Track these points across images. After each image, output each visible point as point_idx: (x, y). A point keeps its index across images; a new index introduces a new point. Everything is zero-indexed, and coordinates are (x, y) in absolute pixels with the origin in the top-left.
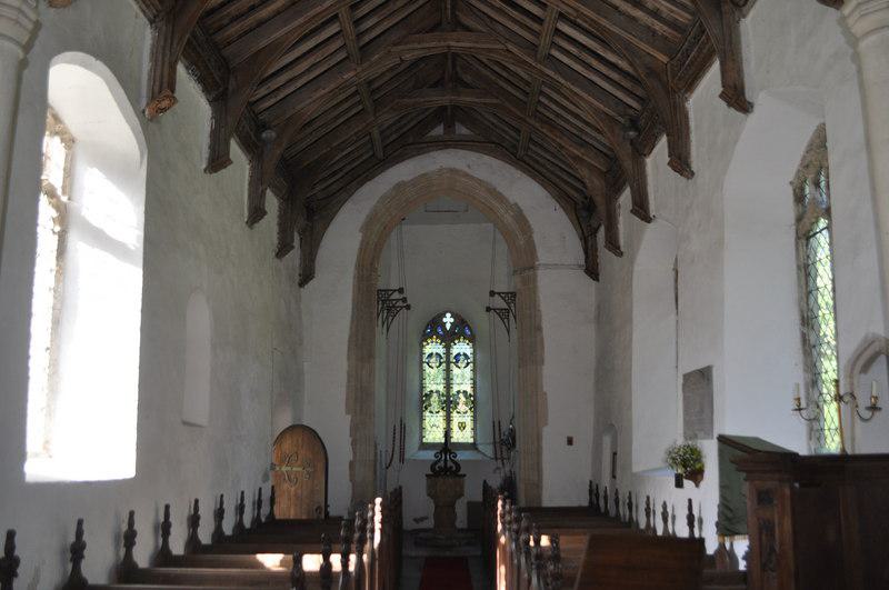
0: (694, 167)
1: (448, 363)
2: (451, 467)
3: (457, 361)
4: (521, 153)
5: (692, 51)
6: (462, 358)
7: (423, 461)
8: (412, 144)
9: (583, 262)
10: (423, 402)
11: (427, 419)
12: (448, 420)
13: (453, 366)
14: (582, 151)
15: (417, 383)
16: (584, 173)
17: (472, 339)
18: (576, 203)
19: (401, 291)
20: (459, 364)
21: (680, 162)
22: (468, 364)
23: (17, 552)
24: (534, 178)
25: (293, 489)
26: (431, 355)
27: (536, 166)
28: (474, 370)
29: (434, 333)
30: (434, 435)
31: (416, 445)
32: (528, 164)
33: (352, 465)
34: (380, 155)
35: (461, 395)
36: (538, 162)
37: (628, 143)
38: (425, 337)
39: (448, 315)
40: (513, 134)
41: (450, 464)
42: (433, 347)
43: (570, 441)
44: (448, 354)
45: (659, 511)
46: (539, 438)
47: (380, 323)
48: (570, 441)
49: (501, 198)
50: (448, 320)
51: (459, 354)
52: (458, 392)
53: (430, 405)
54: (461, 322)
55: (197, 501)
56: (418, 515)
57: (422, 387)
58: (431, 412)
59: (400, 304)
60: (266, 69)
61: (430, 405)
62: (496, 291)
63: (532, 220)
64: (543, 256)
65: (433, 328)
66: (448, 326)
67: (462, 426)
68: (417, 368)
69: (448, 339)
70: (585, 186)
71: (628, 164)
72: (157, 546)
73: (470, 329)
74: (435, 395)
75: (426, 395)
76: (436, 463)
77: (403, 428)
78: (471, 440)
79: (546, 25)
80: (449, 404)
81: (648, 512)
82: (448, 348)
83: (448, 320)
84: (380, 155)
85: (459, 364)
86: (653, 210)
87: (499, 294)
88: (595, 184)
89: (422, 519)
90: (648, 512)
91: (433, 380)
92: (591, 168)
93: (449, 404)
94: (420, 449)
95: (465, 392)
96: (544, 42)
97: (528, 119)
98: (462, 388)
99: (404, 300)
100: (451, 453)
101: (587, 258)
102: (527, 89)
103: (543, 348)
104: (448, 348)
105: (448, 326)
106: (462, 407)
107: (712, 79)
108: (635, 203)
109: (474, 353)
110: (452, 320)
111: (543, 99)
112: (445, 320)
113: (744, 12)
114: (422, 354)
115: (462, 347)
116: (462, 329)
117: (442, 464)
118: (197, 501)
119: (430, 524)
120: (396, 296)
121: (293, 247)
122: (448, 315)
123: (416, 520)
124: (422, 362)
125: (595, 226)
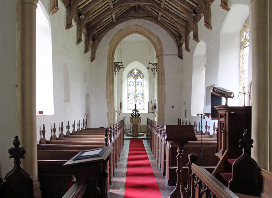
14: (178, 19)
19: (121, 63)
21: (208, 24)
22: (142, 85)
33: (108, 113)
34: (115, 21)
37: (193, 18)
39: (136, 70)
41: (137, 114)
43: (173, 107)
47: (115, 72)
48: (173, 107)
49: (152, 34)
50: (136, 72)
53: (130, 97)
64: (165, 52)
66: (135, 73)
71: (192, 24)
76: (133, 113)
83: (136, 72)
88: (182, 30)
92: (181, 25)
97: (161, 10)
99: (122, 65)
105: (135, 73)
110: (137, 71)
112: (134, 71)
117: (134, 114)
122: (136, 70)
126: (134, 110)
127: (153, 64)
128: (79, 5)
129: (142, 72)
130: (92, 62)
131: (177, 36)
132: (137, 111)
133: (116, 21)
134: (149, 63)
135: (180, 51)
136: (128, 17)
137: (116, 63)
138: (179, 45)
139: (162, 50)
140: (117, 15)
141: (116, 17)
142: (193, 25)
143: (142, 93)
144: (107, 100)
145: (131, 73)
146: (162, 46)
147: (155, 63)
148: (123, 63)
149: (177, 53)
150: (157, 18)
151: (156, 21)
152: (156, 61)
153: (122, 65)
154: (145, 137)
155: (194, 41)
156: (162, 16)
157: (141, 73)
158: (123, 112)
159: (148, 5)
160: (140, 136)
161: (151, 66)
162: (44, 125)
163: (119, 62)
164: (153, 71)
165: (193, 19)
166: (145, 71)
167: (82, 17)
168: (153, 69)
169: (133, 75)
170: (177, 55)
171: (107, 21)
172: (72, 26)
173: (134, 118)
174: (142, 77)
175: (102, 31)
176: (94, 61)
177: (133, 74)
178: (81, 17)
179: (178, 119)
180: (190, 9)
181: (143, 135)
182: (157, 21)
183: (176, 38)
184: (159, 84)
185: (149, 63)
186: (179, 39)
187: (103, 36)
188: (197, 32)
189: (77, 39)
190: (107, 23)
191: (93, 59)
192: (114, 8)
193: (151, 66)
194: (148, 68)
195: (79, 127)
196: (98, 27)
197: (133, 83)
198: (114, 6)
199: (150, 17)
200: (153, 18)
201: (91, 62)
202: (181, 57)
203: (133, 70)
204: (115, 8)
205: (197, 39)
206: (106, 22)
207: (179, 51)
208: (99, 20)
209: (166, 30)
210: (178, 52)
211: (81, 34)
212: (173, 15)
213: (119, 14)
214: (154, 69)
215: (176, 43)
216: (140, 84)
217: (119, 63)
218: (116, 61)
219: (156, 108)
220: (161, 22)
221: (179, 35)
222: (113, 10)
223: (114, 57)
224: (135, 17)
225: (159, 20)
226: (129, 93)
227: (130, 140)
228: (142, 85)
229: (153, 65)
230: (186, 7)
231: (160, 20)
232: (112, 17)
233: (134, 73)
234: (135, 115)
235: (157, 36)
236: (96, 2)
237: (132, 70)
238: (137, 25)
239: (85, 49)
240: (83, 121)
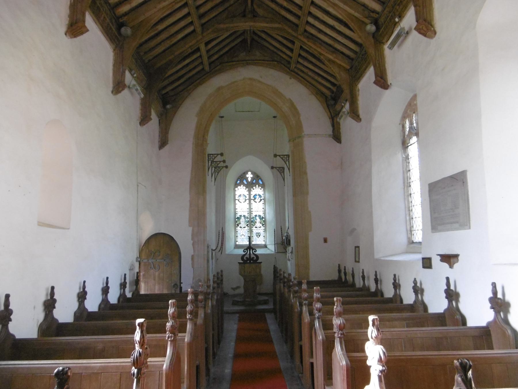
0: (361, 117)
1: (250, 199)
2: (254, 258)
3: (255, 199)
4: (293, 66)
5: (382, 31)
6: (258, 197)
7: (236, 255)
8: (227, 62)
9: (331, 133)
10: (236, 222)
11: (239, 232)
12: (251, 231)
13: (252, 201)
14: (334, 55)
15: (233, 210)
16: (335, 70)
17: (263, 186)
18: (326, 97)
19: (222, 154)
20: (256, 200)
21: (355, 115)
22: (261, 200)
23: (55, 297)
24: (301, 82)
25: (157, 274)
26: (240, 196)
27: (302, 75)
28: (264, 204)
29: (242, 183)
30: (243, 241)
31: (232, 244)
32: (297, 74)
33: (193, 257)
34: (207, 68)
35: (257, 218)
36: (303, 72)
37: (371, 37)
38: (236, 185)
39: (249, 173)
40: (288, 53)
41: (252, 256)
42: (241, 190)
43: (325, 241)
44: (250, 195)
45: (343, 271)
46: (307, 239)
47: (210, 175)
48: (325, 241)
49: (280, 95)
50: (250, 176)
51: (256, 195)
52: (256, 216)
53: (240, 223)
54: (257, 177)
55: (107, 278)
56: (235, 286)
57: (235, 213)
58: (241, 227)
59: (222, 164)
60: (165, 75)
61: (240, 223)
62: (278, 154)
63: (299, 108)
64: (306, 130)
65: (241, 179)
66: (249, 179)
67: (258, 235)
68: (233, 202)
69: (250, 186)
70: (334, 77)
71: (371, 51)
72: (121, 293)
73: (262, 181)
74: (243, 218)
75: (238, 218)
76: (245, 255)
77: (223, 234)
78: (264, 243)
79: (293, 59)
80: (251, 223)
81: (363, 277)
82: (250, 191)
83: (250, 176)
84: (207, 68)
85: (256, 200)
86: (390, 79)
87: (279, 156)
88: (342, 77)
89: (238, 287)
90: (363, 277)
91: (242, 208)
92: (340, 66)
93: (251, 223)
94: (235, 248)
95: (259, 216)
96: (294, 55)
97: (299, 37)
98: (258, 214)
99: (224, 161)
100: (253, 249)
101: (334, 130)
102: (299, 13)
103: (308, 185)
104: (250, 191)
105: (249, 179)
106: (258, 224)
107: (370, 74)
108: (376, 75)
109: (264, 194)
110: (252, 176)
111: (311, 20)
112: (247, 176)
113: (357, 84)
114: (235, 195)
115: (257, 191)
116: (257, 181)
117: (248, 256)
118: (107, 278)
119: (241, 291)
120: (219, 158)
121: (151, 119)
122: (249, 173)
123: (234, 289)
124: (235, 200)
125: (338, 109)
126: (247, 249)
127: (282, 157)
128: (167, 75)
129: (261, 177)
130: (161, 151)
131: (329, 98)
132: (253, 249)
133: (210, 68)
134: (275, 156)
135: (336, 126)
136: (233, 62)
137: (212, 154)
138: (332, 114)
139: (299, 126)
140: (213, 55)
141: (209, 58)
142: (373, 52)
143: (262, 215)
144: (191, 229)
145: (242, 178)
146: (299, 118)
147: (286, 155)
148: (227, 161)
149: (330, 131)
150: (289, 63)
151: (288, 70)
152: (286, 151)
153: (224, 161)
154: (270, 306)
155: (378, 88)
156: (301, 47)
157: (258, 178)
158: (227, 252)
159: (272, 28)
160: (260, 303)
161: (279, 162)
162: (363, 270)
163: (218, 153)
164: (287, 162)
165: (372, 40)
166: (267, 174)
167: (126, 31)
168: (281, 170)
169: (246, 183)
170: (330, 135)
171: (191, 66)
172: (151, 119)
173: (247, 265)
174: (261, 185)
175: (181, 88)
176: (167, 148)
177: (245, 182)
178: (123, 30)
179: (338, 265)
180: (366, 18)
181: (266, 302)
182: (289, 69)
183: (326, 101)
184: (295, 195)
185: (275, 156)
186: (332, 102)
187: (184, 99)
188: (384, 66)
189: (114, 82)
190: (190, 71)
191: (163, 143)
192: (202, 33)
193: (279, 162)
194: (272, 168)
195: (163, 286)
196: (170, 73)
197: (244, 197)
198: (203, 29)
199: (276, 61)
200: (282, 63)
201: (159, 150)
202: (337, 137)
203: (246, 173)
204: (205, 34)
205: (384, 80)
206: (188, 69)
207: (333, 126)
208: (173, 56)
209: (307, 87)
210: (331, 128)
211: (124, 72)
212: (323, 48)
213: (217, 52)
214: (289, 157)
215: (327, 110)
216: (258, 200)
217: (218, 155)
218: (211, 149)
219: (288, 242)
220: (296, 70)
221: (333, 95)
222: (200, 37)
223: (206, 141)
224: (246, 63)
225: (294, 66)
226: (238, 216)
227: (238, 315)
228: (261, 200)
229: (283, 159)
230: (356, 14)
231: (295, 67)
232: (200, 56)
233: (247, 179)
234: (250, 259)
235: (290, 99)
236: (159, 3)
237: (244, 173)
238: (251, 79)
239: (140, 115)
240: (123, 276)
